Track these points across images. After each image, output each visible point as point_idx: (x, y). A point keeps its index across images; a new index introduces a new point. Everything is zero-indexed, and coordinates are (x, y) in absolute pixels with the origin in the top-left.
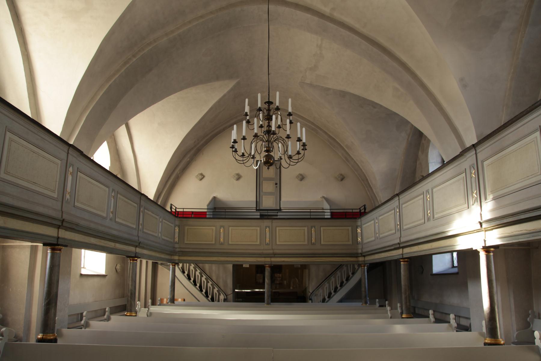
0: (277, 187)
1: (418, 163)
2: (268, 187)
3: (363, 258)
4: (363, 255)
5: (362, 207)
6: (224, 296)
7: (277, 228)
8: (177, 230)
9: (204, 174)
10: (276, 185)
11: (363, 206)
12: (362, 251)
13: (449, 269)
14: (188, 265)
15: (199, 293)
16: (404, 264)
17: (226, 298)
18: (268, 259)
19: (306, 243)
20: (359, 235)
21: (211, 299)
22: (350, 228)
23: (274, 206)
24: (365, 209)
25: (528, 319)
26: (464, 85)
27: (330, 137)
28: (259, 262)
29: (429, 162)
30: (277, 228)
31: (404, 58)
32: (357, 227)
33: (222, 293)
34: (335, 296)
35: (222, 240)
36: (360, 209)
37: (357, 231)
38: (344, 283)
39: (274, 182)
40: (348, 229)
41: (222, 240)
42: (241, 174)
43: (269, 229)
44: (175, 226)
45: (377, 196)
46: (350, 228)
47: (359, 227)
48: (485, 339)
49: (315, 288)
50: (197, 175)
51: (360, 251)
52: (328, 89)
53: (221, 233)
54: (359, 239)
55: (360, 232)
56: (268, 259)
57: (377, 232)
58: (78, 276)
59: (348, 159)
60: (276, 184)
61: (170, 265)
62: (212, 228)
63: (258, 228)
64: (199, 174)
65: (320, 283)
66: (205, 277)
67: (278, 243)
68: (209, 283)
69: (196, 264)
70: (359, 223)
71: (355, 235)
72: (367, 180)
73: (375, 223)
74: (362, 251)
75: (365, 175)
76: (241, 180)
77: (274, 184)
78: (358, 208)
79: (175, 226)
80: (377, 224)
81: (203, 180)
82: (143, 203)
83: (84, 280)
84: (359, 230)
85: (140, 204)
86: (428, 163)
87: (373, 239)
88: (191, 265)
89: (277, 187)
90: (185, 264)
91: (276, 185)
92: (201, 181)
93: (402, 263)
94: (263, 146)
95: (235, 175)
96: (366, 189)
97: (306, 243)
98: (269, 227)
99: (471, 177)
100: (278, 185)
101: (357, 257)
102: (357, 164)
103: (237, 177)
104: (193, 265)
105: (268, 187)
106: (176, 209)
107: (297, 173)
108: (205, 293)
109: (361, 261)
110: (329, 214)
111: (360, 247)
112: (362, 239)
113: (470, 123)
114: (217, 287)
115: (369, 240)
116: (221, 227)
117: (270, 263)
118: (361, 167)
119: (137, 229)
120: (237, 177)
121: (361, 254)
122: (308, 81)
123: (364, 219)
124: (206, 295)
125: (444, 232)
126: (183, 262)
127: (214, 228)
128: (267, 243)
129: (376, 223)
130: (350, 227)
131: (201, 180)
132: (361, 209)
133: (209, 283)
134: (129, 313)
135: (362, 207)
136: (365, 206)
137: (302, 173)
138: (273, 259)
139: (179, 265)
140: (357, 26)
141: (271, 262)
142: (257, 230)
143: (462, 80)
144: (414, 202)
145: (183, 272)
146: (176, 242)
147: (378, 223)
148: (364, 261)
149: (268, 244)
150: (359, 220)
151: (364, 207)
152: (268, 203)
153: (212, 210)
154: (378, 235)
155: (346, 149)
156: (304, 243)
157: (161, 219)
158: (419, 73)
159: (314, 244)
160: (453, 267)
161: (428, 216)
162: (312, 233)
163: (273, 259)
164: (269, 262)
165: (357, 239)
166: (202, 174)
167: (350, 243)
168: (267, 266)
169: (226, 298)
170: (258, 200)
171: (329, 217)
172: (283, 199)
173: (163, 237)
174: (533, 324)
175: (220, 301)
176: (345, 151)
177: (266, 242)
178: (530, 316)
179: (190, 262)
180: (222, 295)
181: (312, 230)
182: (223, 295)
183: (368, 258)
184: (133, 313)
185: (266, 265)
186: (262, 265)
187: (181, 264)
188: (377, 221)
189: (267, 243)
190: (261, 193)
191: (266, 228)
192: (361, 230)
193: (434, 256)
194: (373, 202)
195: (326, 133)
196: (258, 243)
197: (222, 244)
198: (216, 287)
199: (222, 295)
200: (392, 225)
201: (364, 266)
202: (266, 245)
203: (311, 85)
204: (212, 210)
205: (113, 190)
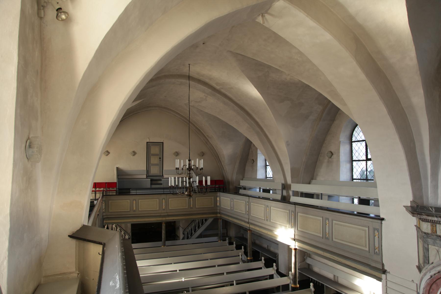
0: (160, 160)
1: (250, 150)
2: (154, 160)
6: (128, 236)
7: (170, 199)
9: (109, 151)
16: (250, 232)
18: (164, 219)
19: (187, 207)
22: (213, 197)
23: (159, 173)
25: (305, 257)
26: (288, 144)
27: (197, 128)
28: (158, 220)
29: (258, 153)
30: (170, 199)
31: (258, 120)
32: (217, 197)
33: (127, 234)
34: (198, 231)
35: (135, 209)
39: (159, 157)
40: (212, 198)
41: (135, 209)
42: (136, 151)
43: (165, 200)
45: (224, 167)
46: (213, 197)
47: (218, 197)
48: (292, 285)
49: (186, 227)
50: (104, 152)
54: (218, 204)
56: (164, 219)
59: (206, 141)
60: (160, 158)
63: (158, 200)
64: (106, 151)
66: (124, 232)
67: (170, 208)
68: (118, 228)
72: (218, 156)
75: (217, 154)
76: (136, 155)
77: (159, 158)
81: (109, 155)
84: (218, 199)
86: (257, 154)
89: (160, 160)
91: (160, 159)
92: (107, 156)
93: (248, 232)
94: (222, 237)
95: (132, 152)
96: (217, 161)
97: (187, 207)
98: (165, 199)
99: (292, 214)
100: (161, 159)
102: (213, 147)
103: (133, 154)
107: (174, 151)
109: (219, 216)
113: (288, 161)
114: (123, 231)
117: (165, 221)
118: (215, 149)
120: (133, 154)
128: (163, 209)
129: (232, 201)
130: (213, 196)
131: (107, 155)
133: (118, 228)
137: (177, 151)
138: (167, 218)
140: (234, 99)
141: (166, 220)
142: (157, 201)
143: (287, 142)
144: (259, 206)
146: (104, 211)
149: (164, 210)
155: (207, 138)
158: (265, 129)
159: (192, 208)
163: (167, 218)
164: (164, 220)
165: (217, 204)
166: (107, 151)
167: (213, 206)
168: (163, 223)
172: (164, 169)
174: (306, 259)
176: (206, 138)
177: (163, 208)
178: (306, 256)
180: (127, 235)
182: (128, 235)
185: (163, 222)
186: (160, 222)
189: (163, 209)
191: (163, 200)
192: (220, 199)
194: (221, 170)
195: (194, 126)
196: (158, 209)
197: (134, 211)
198: (123, 231)
199: (127, 235)
200: (243, 209)
201: (220, 219)
202: (163, 210)
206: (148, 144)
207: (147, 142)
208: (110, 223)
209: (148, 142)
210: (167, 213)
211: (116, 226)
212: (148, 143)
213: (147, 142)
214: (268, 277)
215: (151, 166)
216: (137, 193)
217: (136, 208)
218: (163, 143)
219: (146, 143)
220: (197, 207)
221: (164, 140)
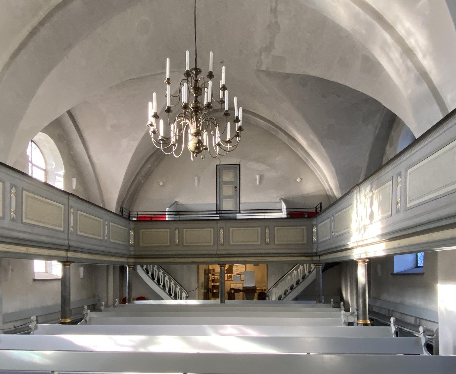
2: (228, 191)
3: (318, 257)
4: (318, 254)
5: (318, 205)
6: (186, 294)
8: (132, 233)
10: (235, 188)
11: (319, 204)
12: (317, 250)
13: (411, 269)
14: (151, 266)
15: (162, 291)
17: (187, 296)
20: (315, 234)
21: (174, 297)
24: (321, 207)
32: (313, 226)
33: (184, 291)
35: (177, 241)
36: (316, 207)
37: (313, 230)
38: (294, 287)
41: (177, 241)
44: (130, 229)
47: (315, 227)
51: (315, 251)
52: (287, 76)
53: (223, 239)
55: (316, 231)
57: (333, 230)
58: (31, 281)
60: (236, 187)
61: (127, 267)
62: (167, 230)
65: (278, 280)
69: (159, 266)
70: (315, 222)
71: (310, 234)
73: (331, 221)
74: (317, 250)
78: (315, 207)
79: (130, 229)
80: (333, 222)
82: (71, 203)
83: (37, 284)
84: (314, 230)
85: (68, 205)
87: (329, 237)
88: (155, 267)
89: (236, 190)
90: (149, 266)
98: (223, 228)
100: (237, 189)
101: (312, 256)
104: (156, 266)
105: (228, 191)
106: (129, 213)
108: (168, 291)
110: (286, 213)
111: (315, 246)
112: (317, 238)
115: (324, 239)
116: (176, 228)
119: (67, 232)
121: (316, 253)
122: (264, 68)
123: (320, 218)
124: (169, 293)
125: (345, 245)
126: (147, 264)
127: (168, 230)
128: (221, 243)
130: (305, 226)
132: (318, 207)
133: (166, 277)
134: (63, 320)
135: (318, 205)
136: (321, 204)
139: (143, 267)
145: (148, 273)
147: (334, 220)
148: (319, 260)
150: (315, 219)
151: (320, 205)
152: (228, 205)
153: (173, 213)
154: (333, 233)
156: (257, 243)
157: (106, 222)
160: (417, 267)
161: (398, 206)
162: (265, 232)
165: (313, 239)
169: (187, 296)
170: (218, 204)
171: (286, 216)
173: (111, 241)
175: (183, 298)
179: (153, 264)
181: (265, 230)
182: (185, 293)
183: (322, 258)
184: (68, 319)
187: (145, 266)
188: (333, 219)
189: (221, 243)
190: (221, 197)
192: (317, 230)
193: (395, 256)
197: (177, 245)
199: (184, 292)
203: (268, 73)
204: (173, 213)
205: (12, 186)
206: (218, 169)
207: (217, 165)
208: (147, 264)
209: (219, 164)
210: (179, 217)
211: (169, 278)
212: (218, 166)
213: (217, 165)
214: (142, 182)
215: (223, 200)
216: (181, 219)
217: (179, 241)
218: (239, 165)
219: (216, 166)
220: (276, 243)
221: (241, 161)
